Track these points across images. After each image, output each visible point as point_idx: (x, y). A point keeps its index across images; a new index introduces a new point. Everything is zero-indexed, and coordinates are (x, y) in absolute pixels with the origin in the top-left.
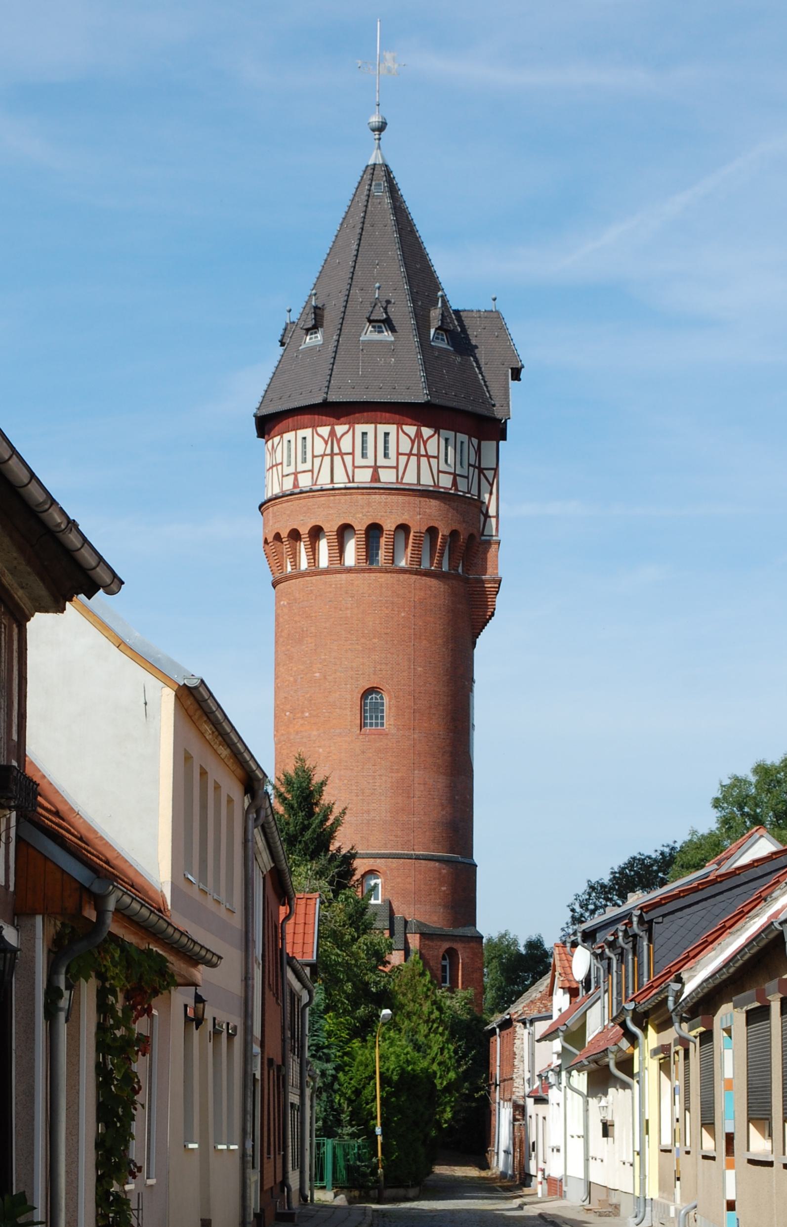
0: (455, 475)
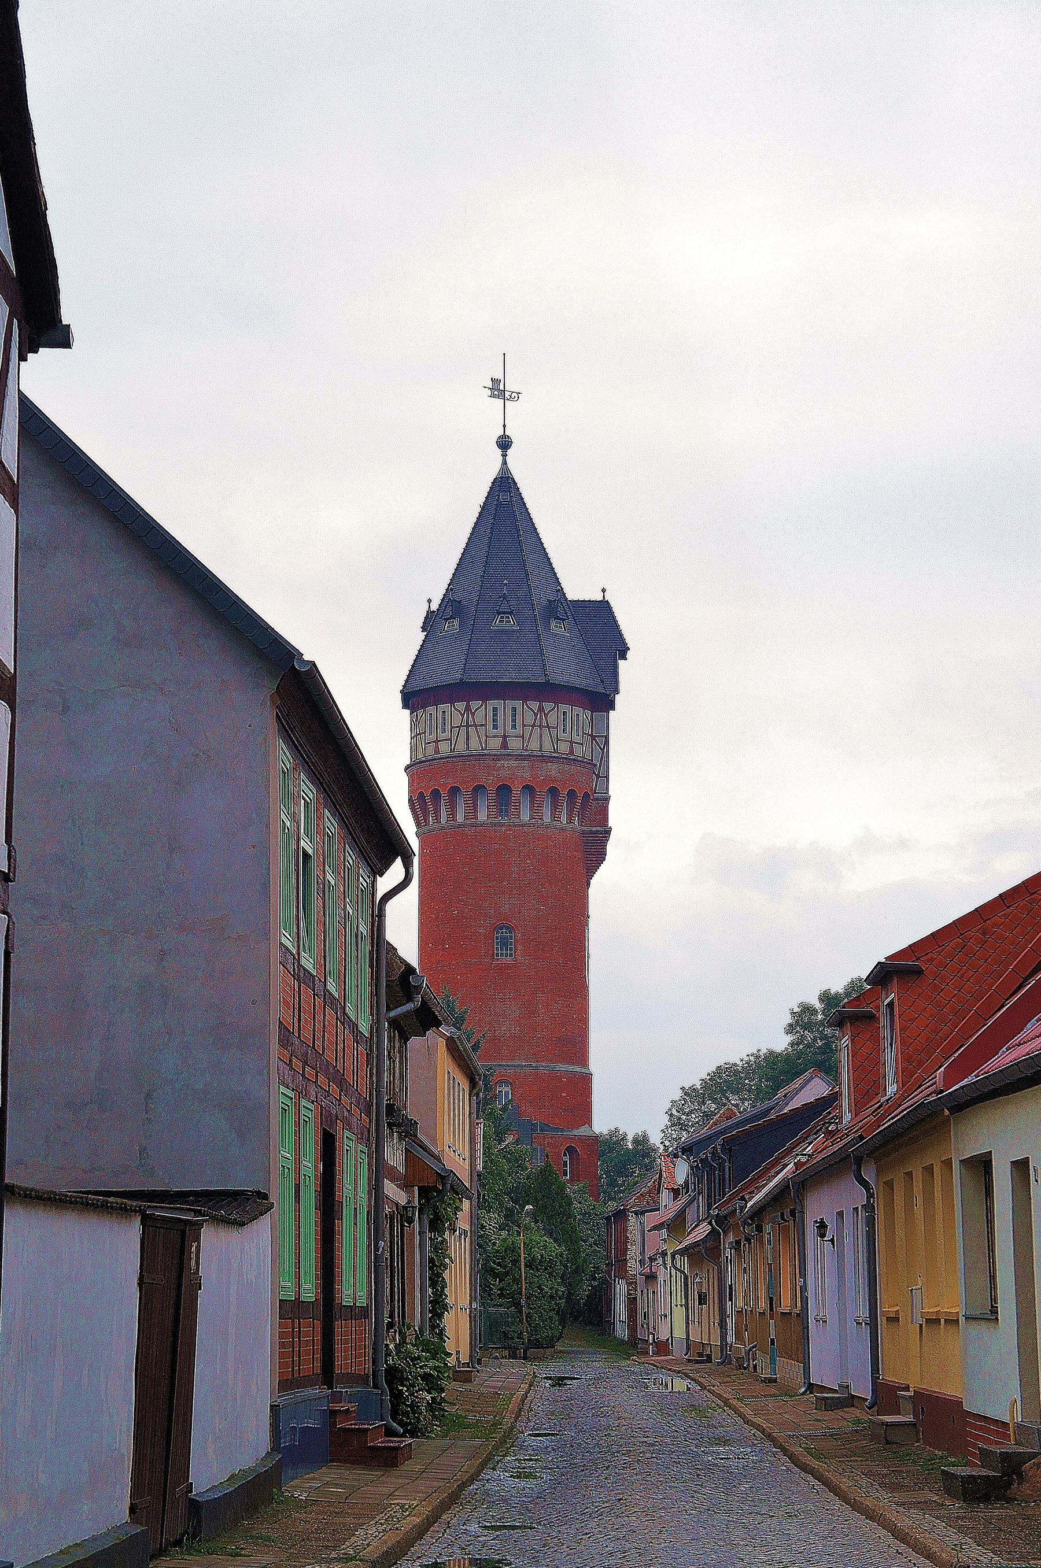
0: (572, 742)
